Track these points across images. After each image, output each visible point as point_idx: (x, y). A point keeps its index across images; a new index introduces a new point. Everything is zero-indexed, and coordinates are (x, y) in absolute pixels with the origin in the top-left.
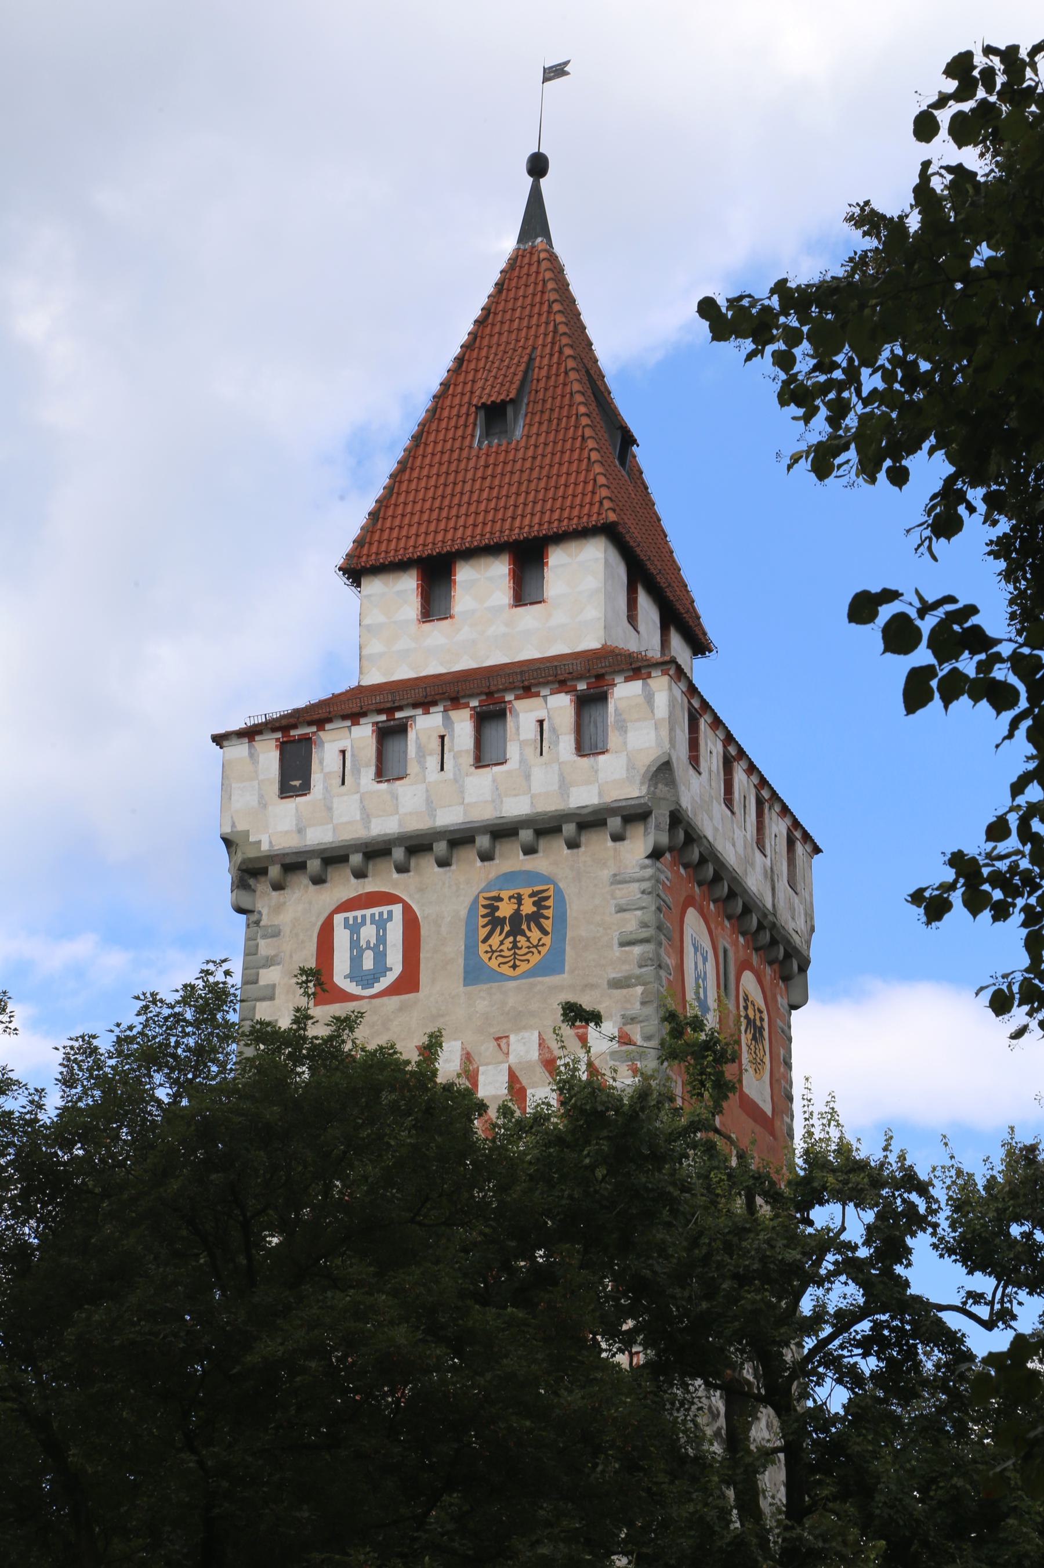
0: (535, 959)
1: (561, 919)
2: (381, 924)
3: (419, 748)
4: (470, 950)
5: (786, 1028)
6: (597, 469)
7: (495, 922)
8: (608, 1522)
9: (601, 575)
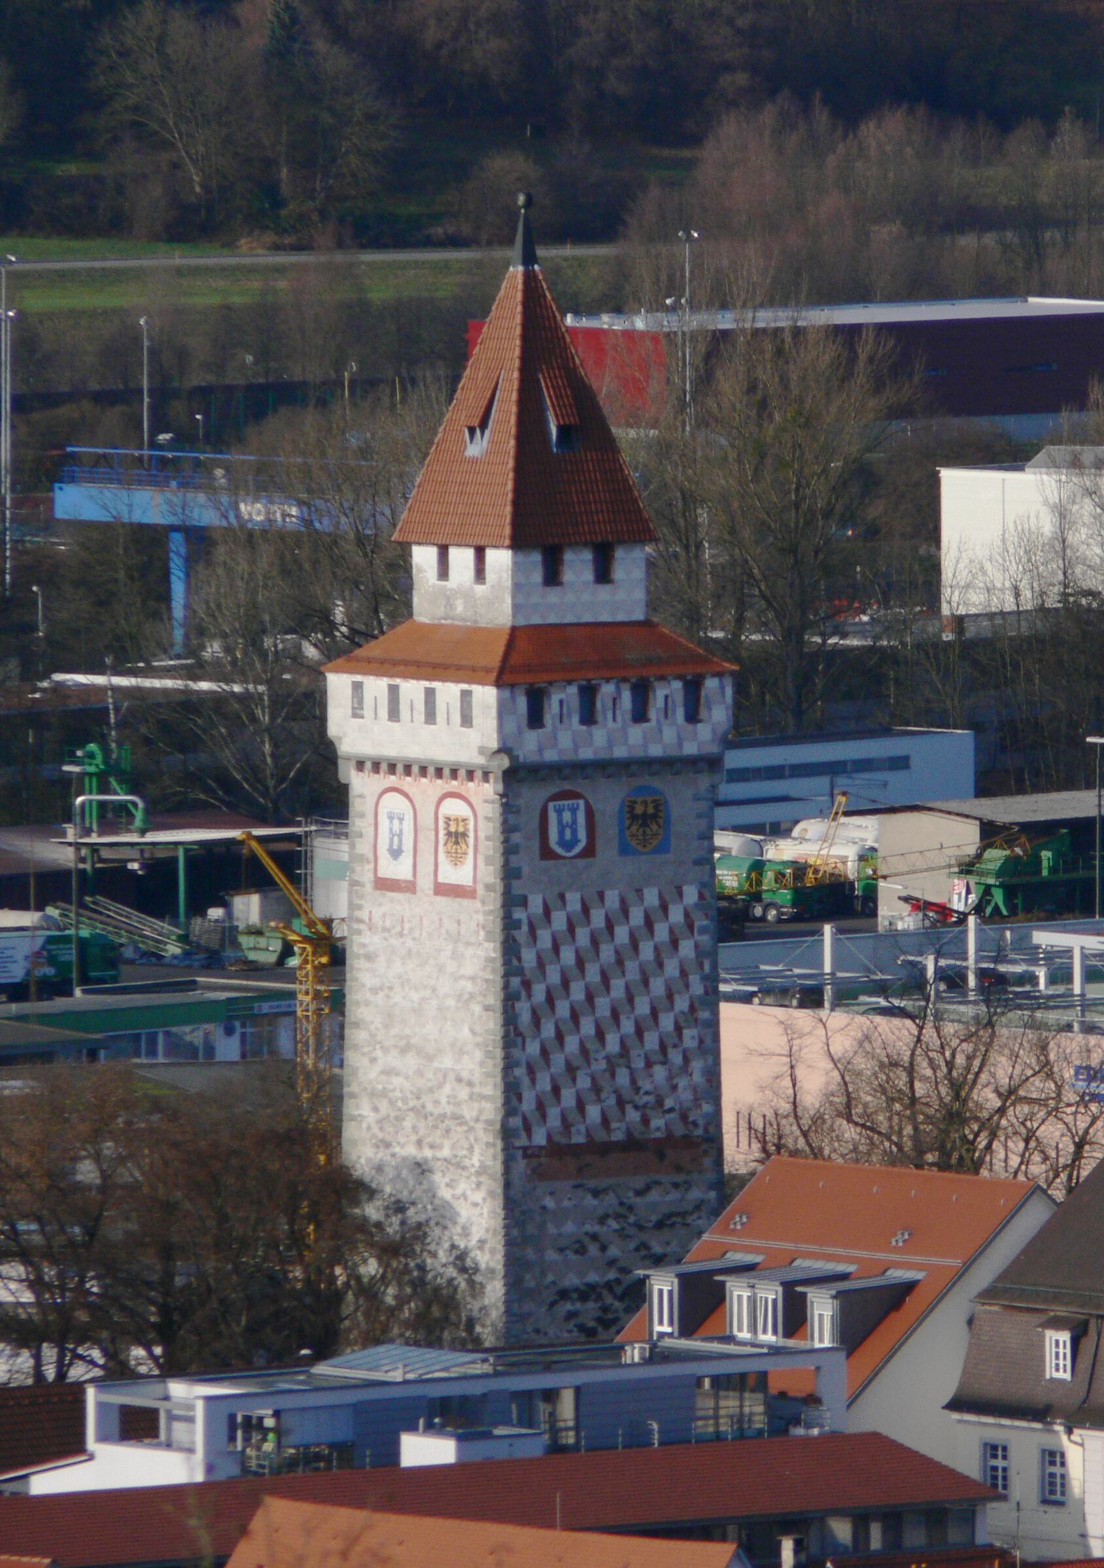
0: (655, 842)
1: (668, 821)
2: (574, 811)
3: (603, 706)
4: (621, 831)
7: (634, 817)
9: (644, 569)
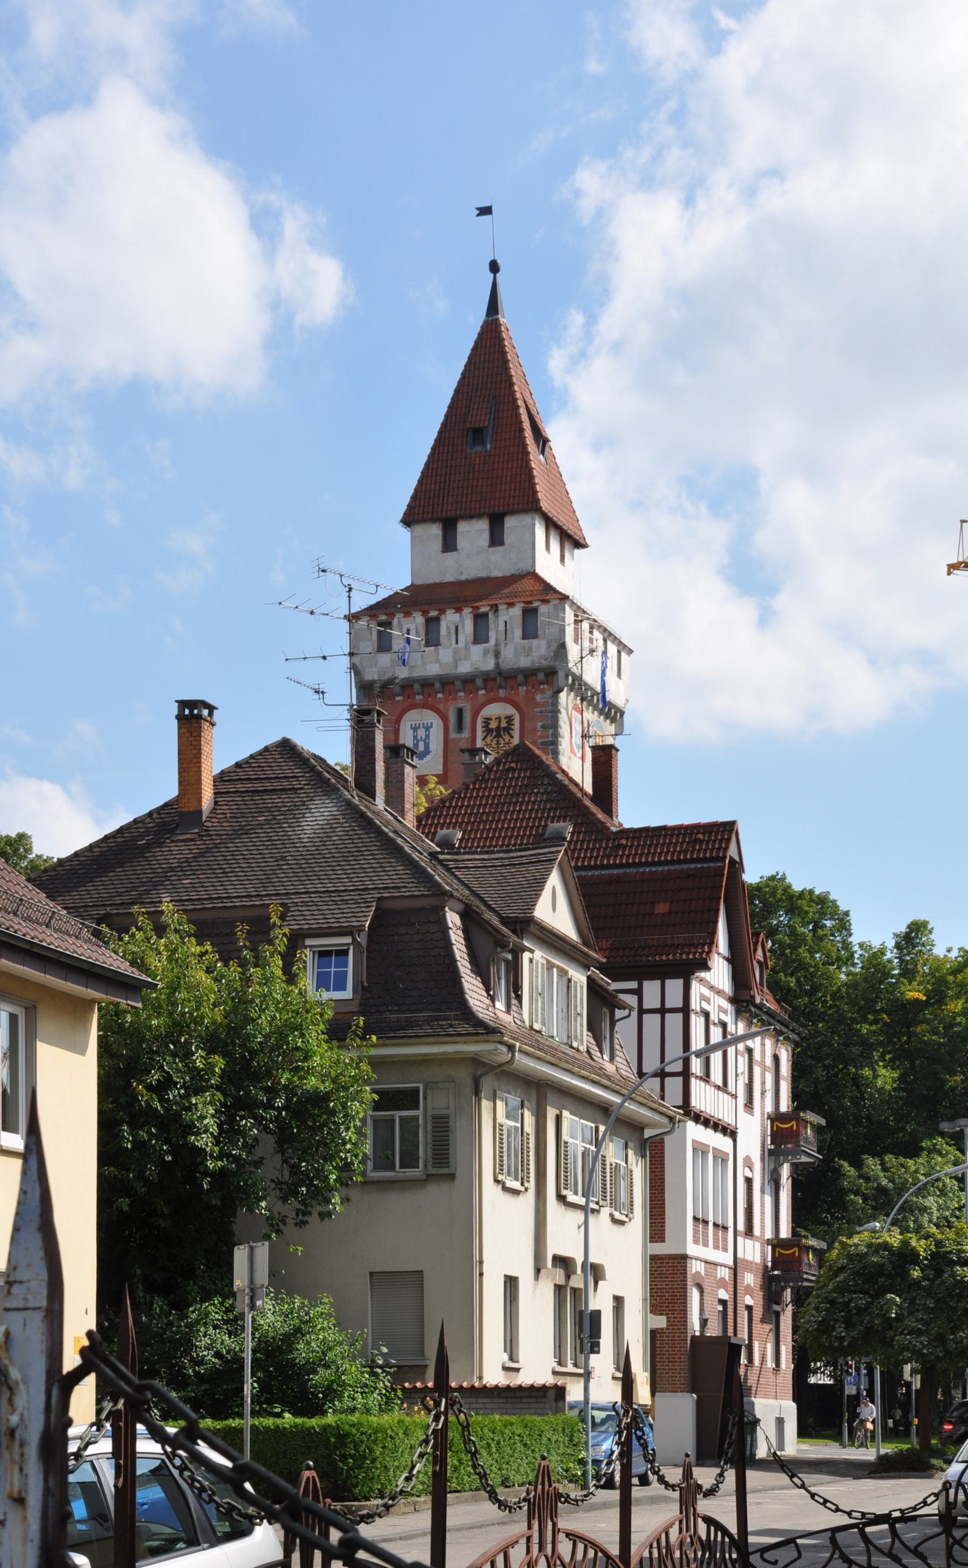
5: (571, 514)
6: (664, 958)
8: (852, 1197)
